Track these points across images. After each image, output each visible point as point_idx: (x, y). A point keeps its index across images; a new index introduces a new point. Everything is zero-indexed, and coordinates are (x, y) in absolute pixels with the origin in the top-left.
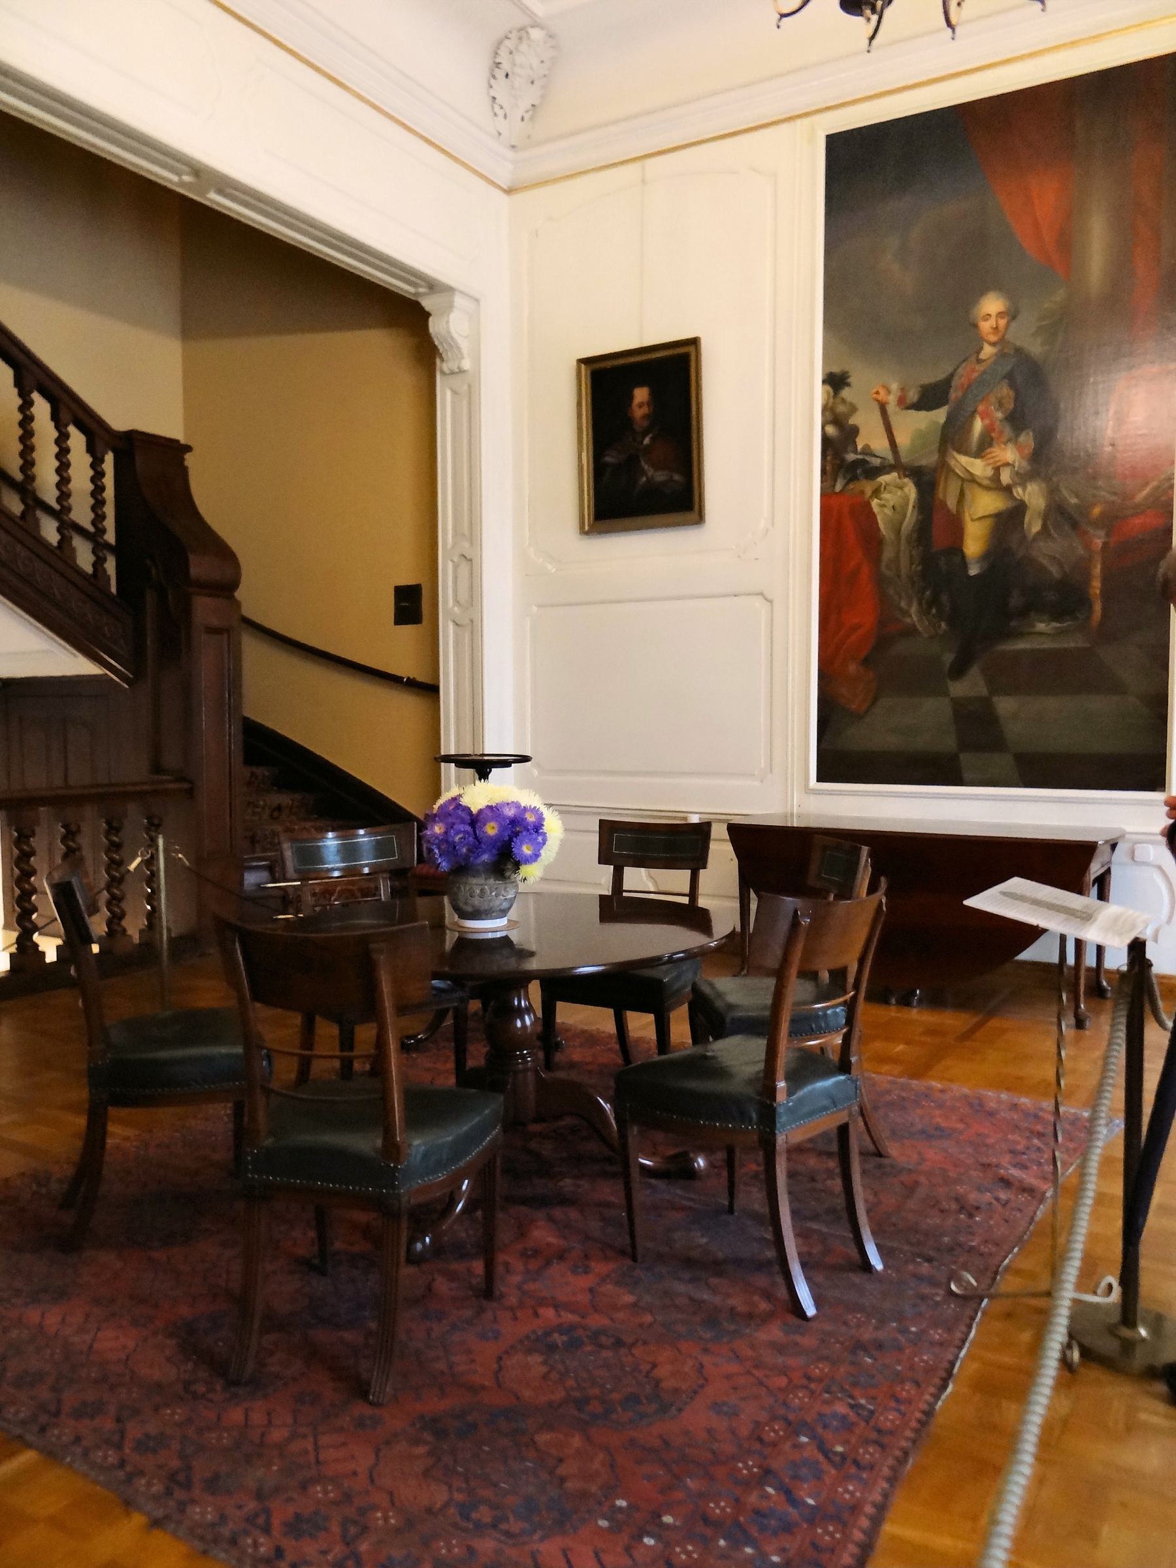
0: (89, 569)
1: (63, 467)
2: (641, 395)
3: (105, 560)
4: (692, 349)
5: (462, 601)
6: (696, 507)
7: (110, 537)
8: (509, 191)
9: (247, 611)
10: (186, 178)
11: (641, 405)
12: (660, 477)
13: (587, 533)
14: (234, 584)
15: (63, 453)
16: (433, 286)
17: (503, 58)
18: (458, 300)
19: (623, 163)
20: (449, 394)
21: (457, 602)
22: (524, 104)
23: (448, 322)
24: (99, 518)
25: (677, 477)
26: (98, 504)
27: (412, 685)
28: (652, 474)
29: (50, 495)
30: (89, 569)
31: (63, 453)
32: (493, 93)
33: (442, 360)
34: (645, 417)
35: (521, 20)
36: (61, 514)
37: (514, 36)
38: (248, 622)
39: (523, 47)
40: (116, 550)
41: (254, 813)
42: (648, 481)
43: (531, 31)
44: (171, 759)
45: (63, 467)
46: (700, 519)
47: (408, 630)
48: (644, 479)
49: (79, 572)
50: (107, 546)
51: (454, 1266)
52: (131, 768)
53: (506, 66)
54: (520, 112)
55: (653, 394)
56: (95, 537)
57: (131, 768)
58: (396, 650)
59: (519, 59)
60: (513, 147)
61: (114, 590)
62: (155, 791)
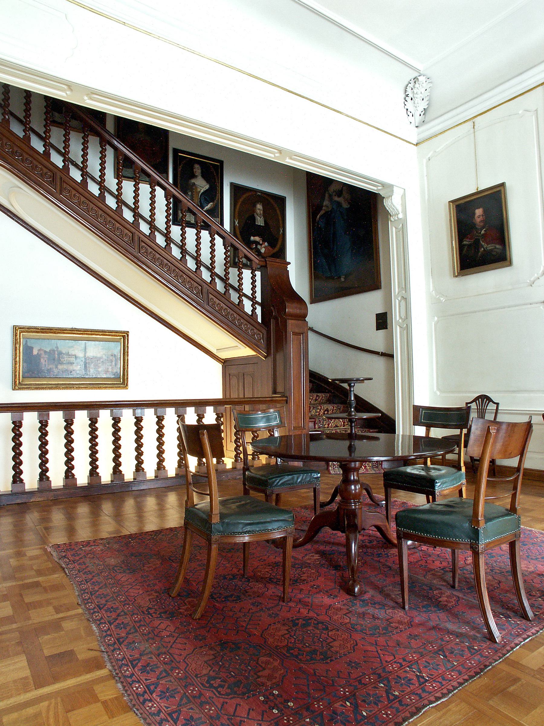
0: (250, 313)
1: (213, 251)
2: (479, 212)
3: (256, 309)
4: (502, 188)
5: (403, 317)
6: (509, 259)
7: (259, 299)
8: (417, 145)
9: (310, 325)
10: (277, 155)
11: (479, 217)
12: (490, 247)
13: (457, 276)
14: (305, 316)
15: (213, 245)
16: (383, 185)
17: (409, 91)
18: (395, 189)
19: (464, 122)
20: (394, 229)
21: (400, 317)
22: (420, 109)
23: (391, 199)
24: (254, 292)
25: (498, 246)
26: (254, 287)
27: (383, 354)
28: (486, 246)
29: (146, 214)
30: (250, 313)
31: (213, 245)
32: (406, 107)
33: (391, 216)
34: (481, 221)
35: (416, 74)
36: (211, 269)
37: (412, 82)
38: (312, 329)
39: (417, 85)
40: (262, 305)
41: (316, 412)
42: (484, 250)
43: (419, 78)
44: (280, 389)
45: (213, 251)
46: (510, 264)
47: (381, 332)
48: (482, 249)
49: (246, 314)
50: (257, 303)
51: (300, 562)
52: (265, 391)
53: (411, 95)
54: (419, 112)
55: (484, 211)
56: (252, 299)
57: (265, 391)
58: (376, 340)
59: (415, 90)
60: (417, 127)
61: (260, 320)
62: (272, 400)
